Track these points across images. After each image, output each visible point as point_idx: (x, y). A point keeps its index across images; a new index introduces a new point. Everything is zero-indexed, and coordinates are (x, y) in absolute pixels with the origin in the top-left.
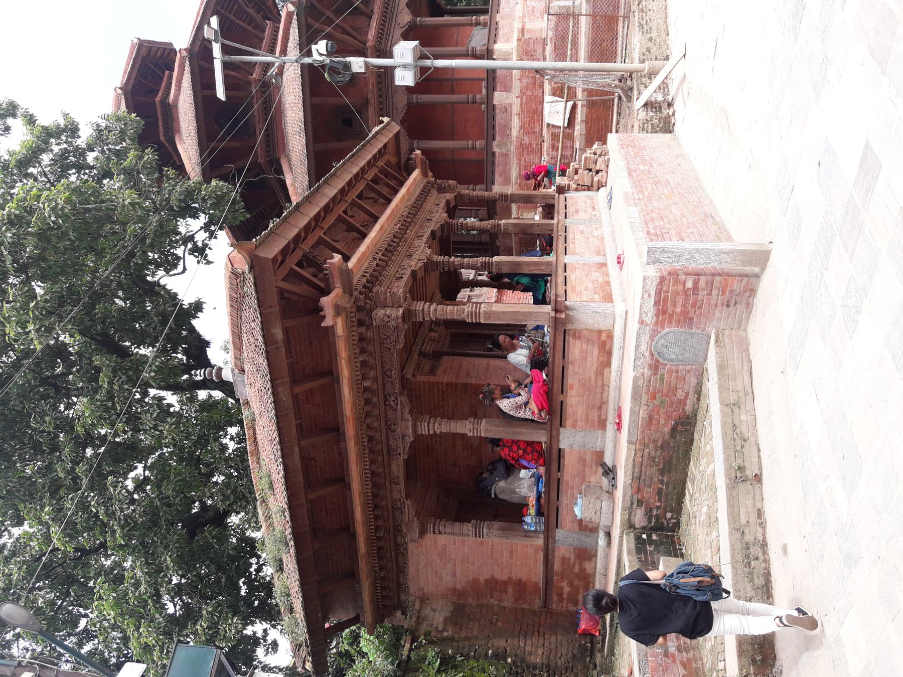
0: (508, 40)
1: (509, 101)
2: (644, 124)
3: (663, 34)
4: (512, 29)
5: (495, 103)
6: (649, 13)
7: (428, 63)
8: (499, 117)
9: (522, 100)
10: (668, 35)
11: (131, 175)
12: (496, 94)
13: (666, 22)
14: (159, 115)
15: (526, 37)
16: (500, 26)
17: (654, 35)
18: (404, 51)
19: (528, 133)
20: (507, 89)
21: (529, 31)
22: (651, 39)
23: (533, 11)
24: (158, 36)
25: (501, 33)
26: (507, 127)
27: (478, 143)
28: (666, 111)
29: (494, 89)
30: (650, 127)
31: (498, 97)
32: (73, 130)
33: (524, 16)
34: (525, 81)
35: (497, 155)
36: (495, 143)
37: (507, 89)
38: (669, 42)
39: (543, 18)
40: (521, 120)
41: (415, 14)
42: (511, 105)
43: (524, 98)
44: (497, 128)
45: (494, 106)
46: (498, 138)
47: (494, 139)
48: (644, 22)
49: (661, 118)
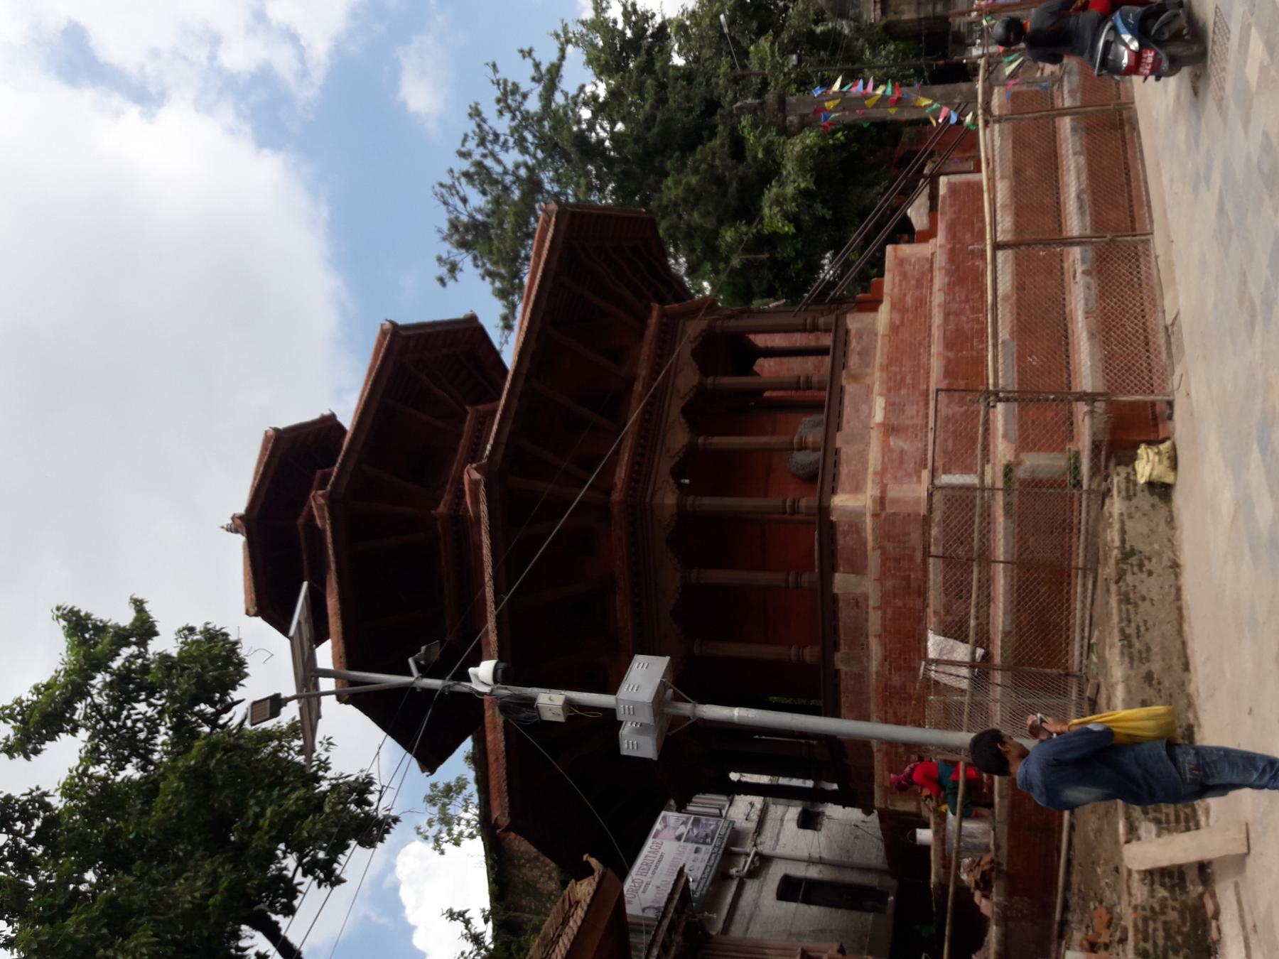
0: (857, 488)
1: (862, 589)
2: (1145, 920)
3: (1177, 665)
4: (865, 464)
5: (836, 591)
6: (1144, 606)
7: (686, 708)
8: (845, 614)
9: (884, 613)
10: (1186, 667)
11: (145, 930)
12: (839, 578)
13: (1180, 631)
14: (303, 544)
15: (889, 510)
16: (843, 457)
17: (1156, 666)
18: (644, 677)
19: (898, 669)
20: (858, 568)
21: (895, 501)
22: (1149, 677)
23: (901, 462)
24: (299, 410)
25: (844, 470)
26: (859, 632)
27: (807, 651)
28: (1195, 889)
29: (834, 569)
30: (1161, 934)
31: (842, 582)
32: (144, 629)
33: (884, 471)
34: (889, 583)
35: (843, 676)
36: (838, 656)
37: (858, 568)
38: (1191, 689)
39: (919, 477)
40: (884, 646)
41: (704, 370)
42: (866, 597)
43: (889, 611)
44: (841, 631)
45: (835, 598)
46: (843, 648)
47: (836, 647)
48: (1131, 630)
49: (1183, 903)
